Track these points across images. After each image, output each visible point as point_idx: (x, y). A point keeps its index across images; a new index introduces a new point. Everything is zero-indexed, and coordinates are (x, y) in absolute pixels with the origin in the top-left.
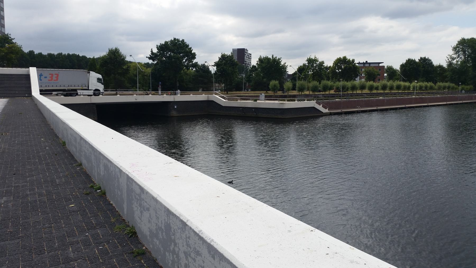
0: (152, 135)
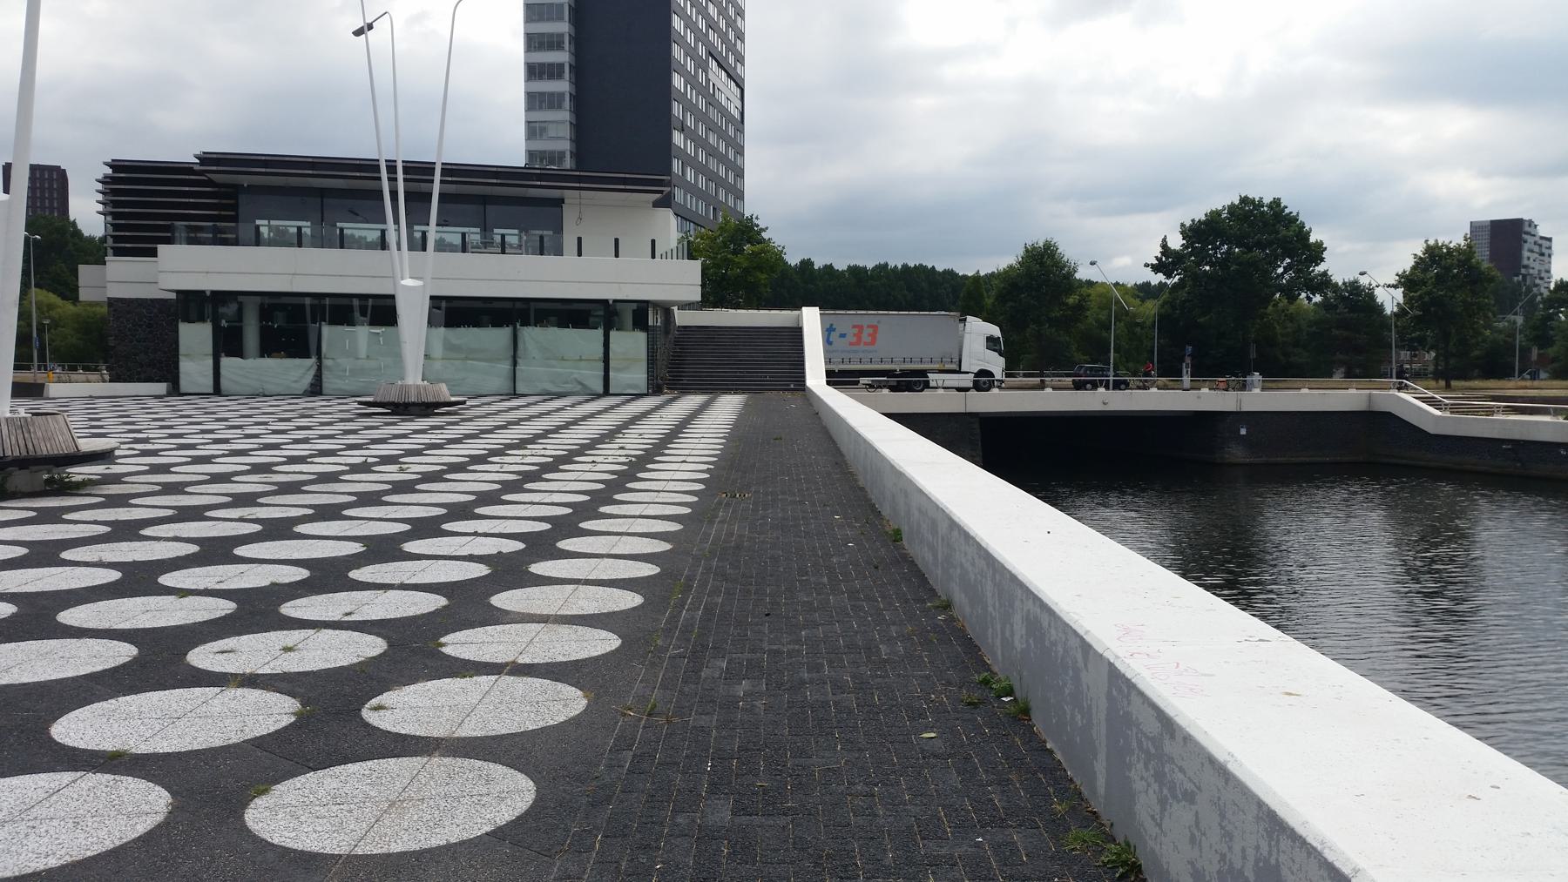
0: (1158, 523)
